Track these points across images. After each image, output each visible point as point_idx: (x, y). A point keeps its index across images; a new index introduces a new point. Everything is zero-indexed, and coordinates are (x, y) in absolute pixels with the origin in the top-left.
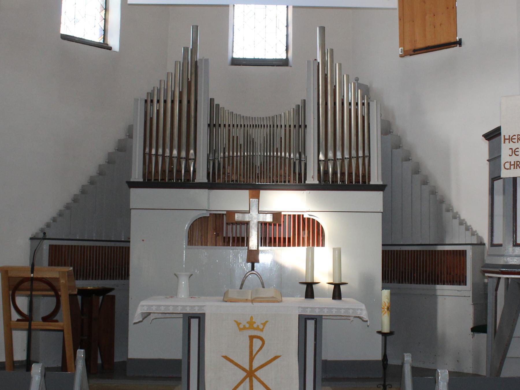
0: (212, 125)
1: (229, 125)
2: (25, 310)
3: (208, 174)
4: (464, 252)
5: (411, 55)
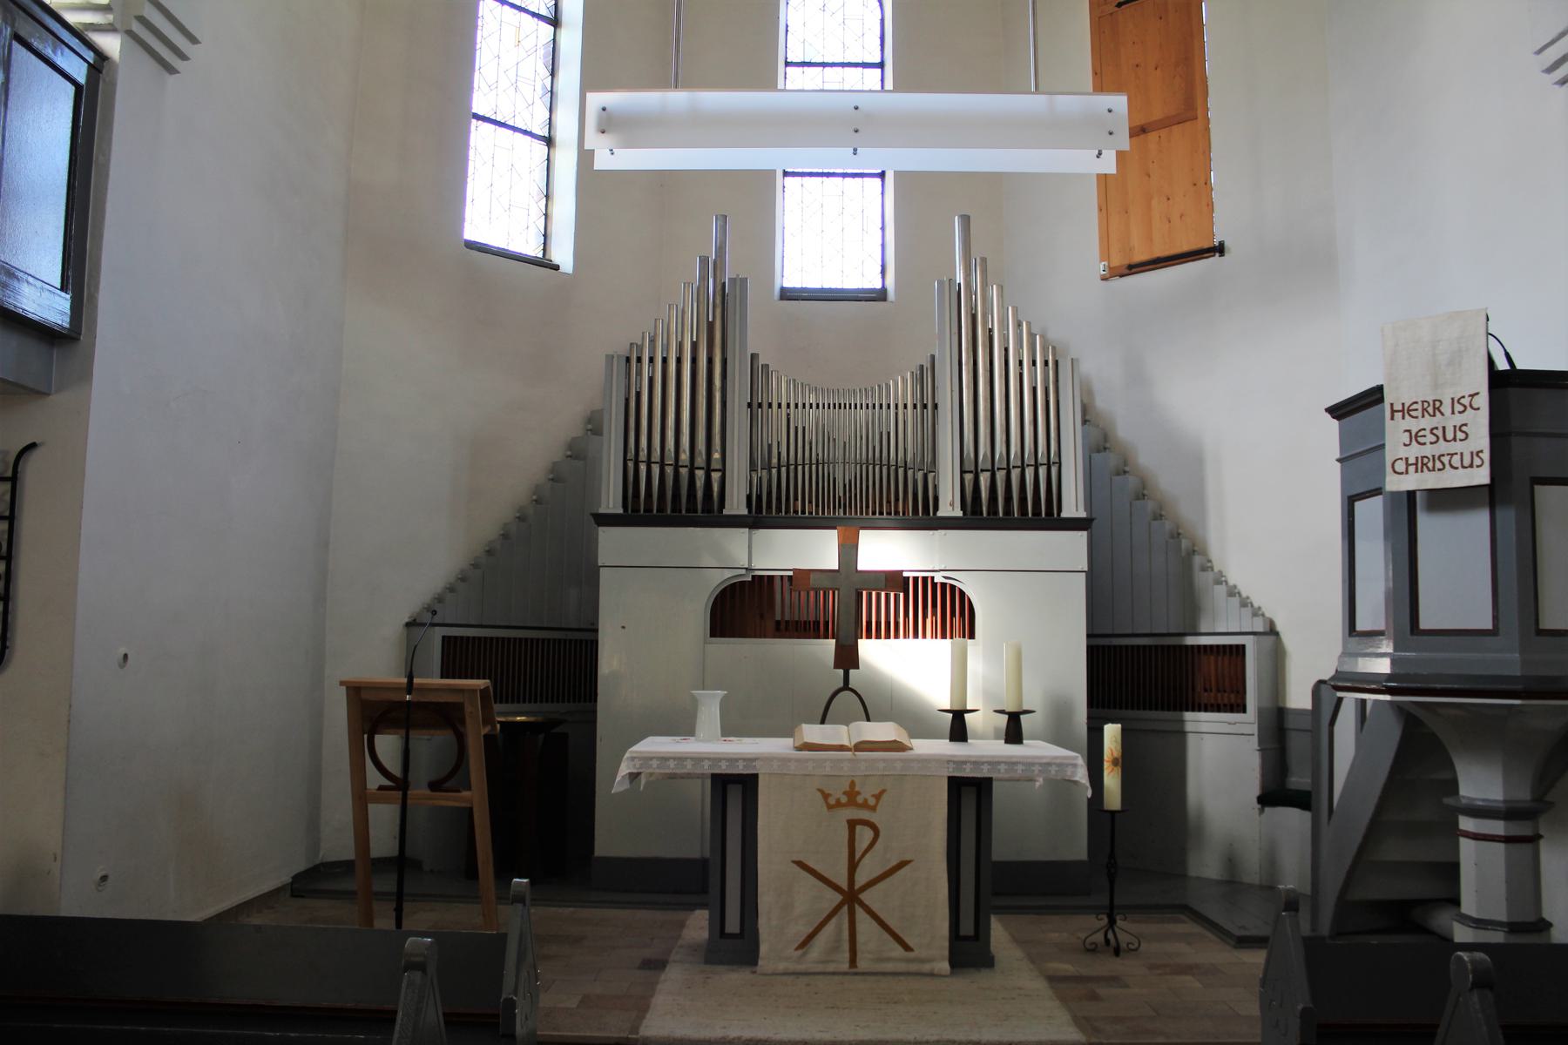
0: (755, 405)
1: (788, 406)
2: (395, 768)
3: (749, 498)
4: (1240, 649)
5: (1122, 276)
